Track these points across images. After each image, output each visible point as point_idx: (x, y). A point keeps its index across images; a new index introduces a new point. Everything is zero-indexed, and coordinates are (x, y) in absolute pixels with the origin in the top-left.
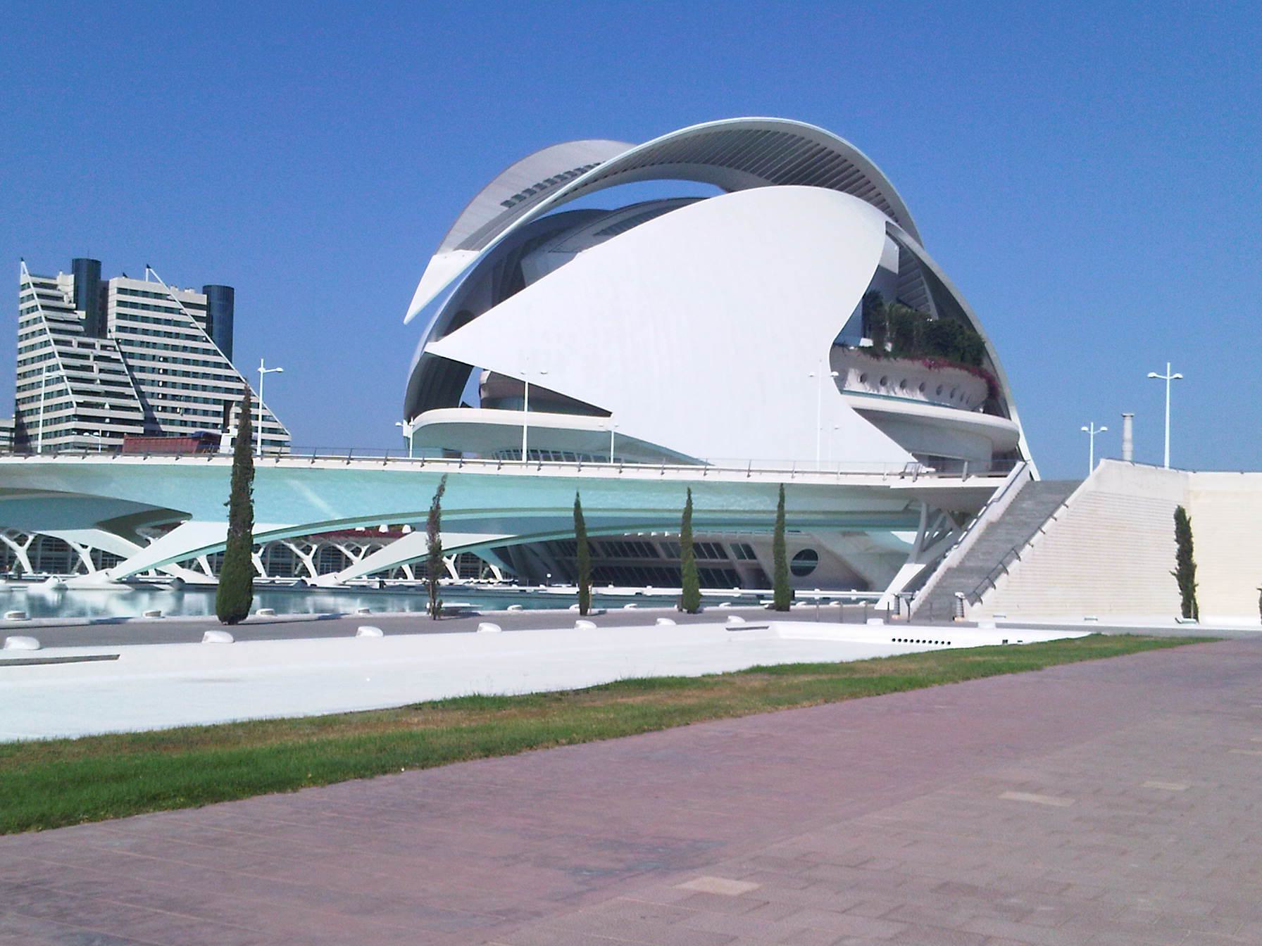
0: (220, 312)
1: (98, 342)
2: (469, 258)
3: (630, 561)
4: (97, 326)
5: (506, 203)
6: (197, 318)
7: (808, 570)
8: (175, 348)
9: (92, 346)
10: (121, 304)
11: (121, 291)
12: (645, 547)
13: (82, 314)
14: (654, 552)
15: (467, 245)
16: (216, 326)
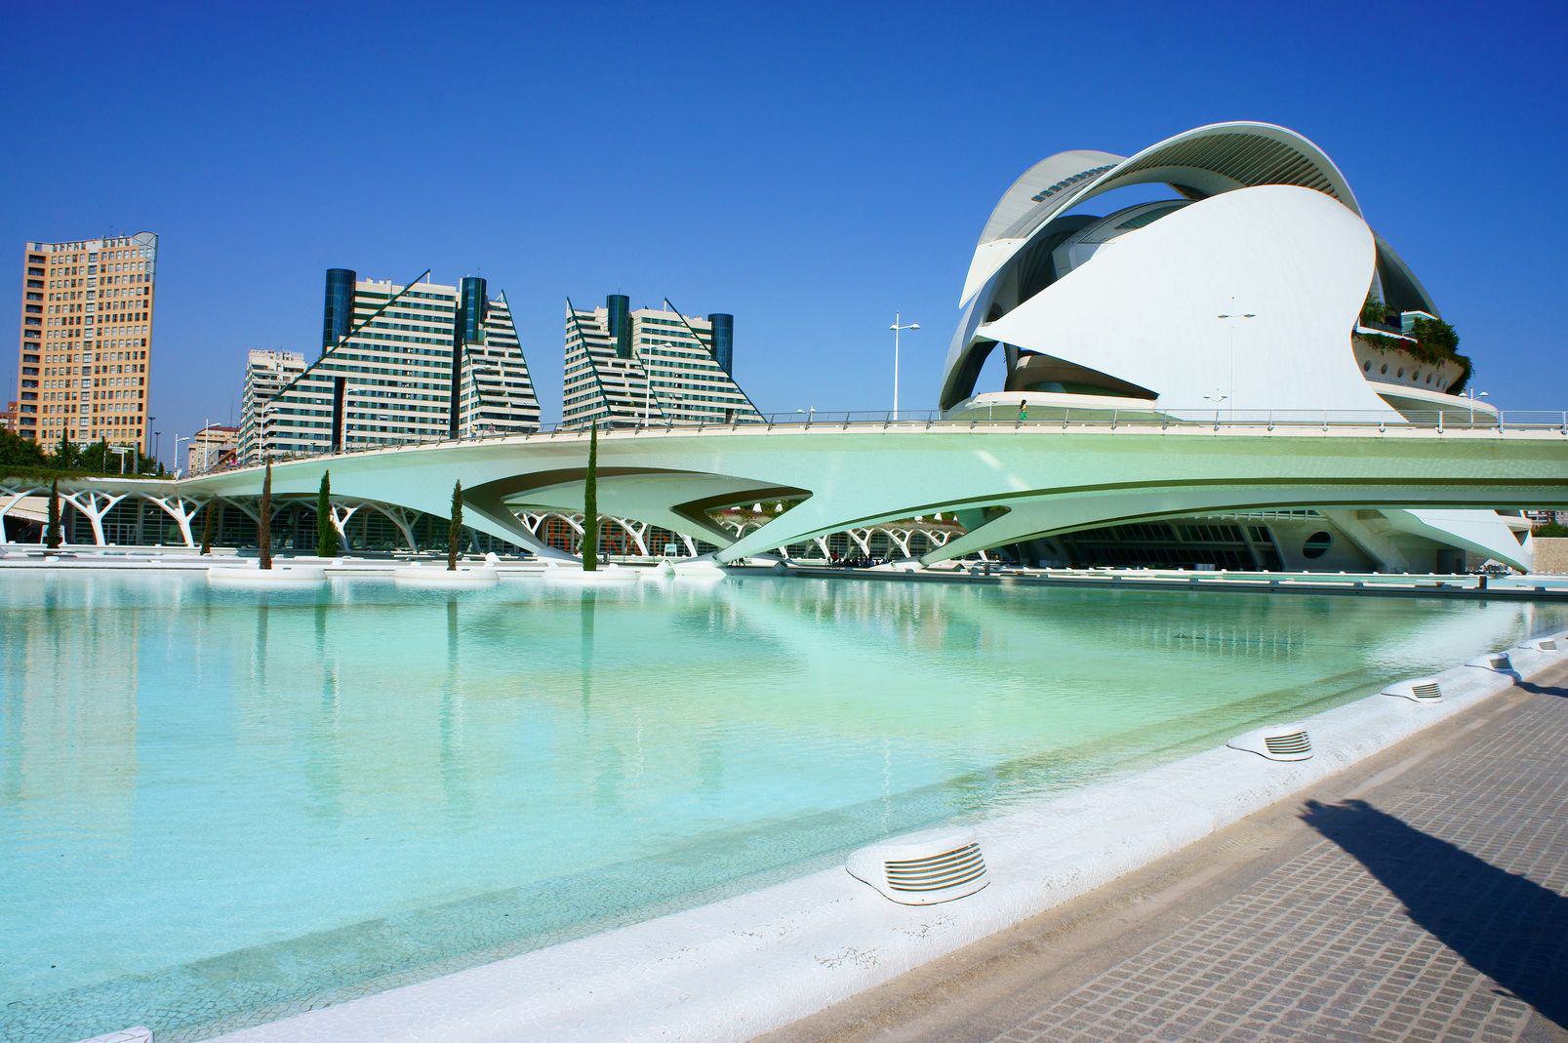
0: (721, 335)
1: (628, 362)
2: (1015, 245)
3: (1157, 542)
4: (625, 350)
5: (1037, 198)
6: (704, 342)
7: (1321, 552)
8: (688, 366)
9: (623, 366)
10: (645, 330)
11: (646, 320)
12: (1231, 530)
13: (614, 340)
14: (1239, 536)
15: (1011, 233)
16: (720, 348)
